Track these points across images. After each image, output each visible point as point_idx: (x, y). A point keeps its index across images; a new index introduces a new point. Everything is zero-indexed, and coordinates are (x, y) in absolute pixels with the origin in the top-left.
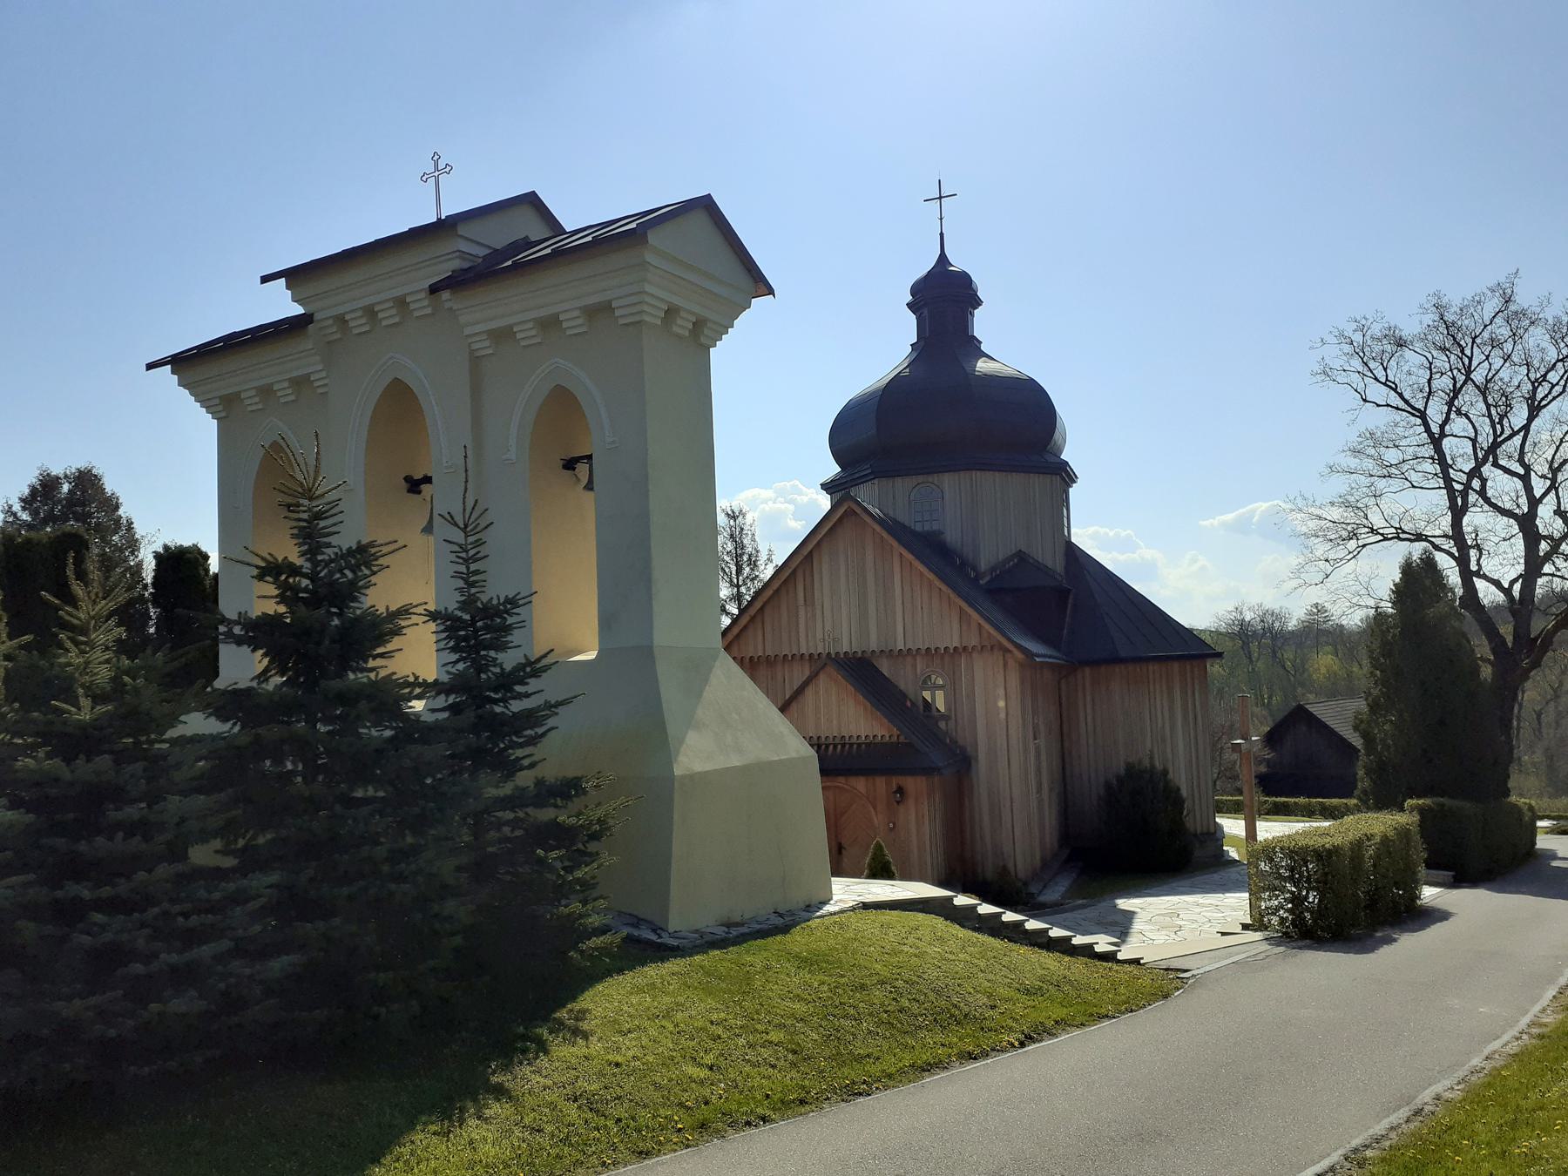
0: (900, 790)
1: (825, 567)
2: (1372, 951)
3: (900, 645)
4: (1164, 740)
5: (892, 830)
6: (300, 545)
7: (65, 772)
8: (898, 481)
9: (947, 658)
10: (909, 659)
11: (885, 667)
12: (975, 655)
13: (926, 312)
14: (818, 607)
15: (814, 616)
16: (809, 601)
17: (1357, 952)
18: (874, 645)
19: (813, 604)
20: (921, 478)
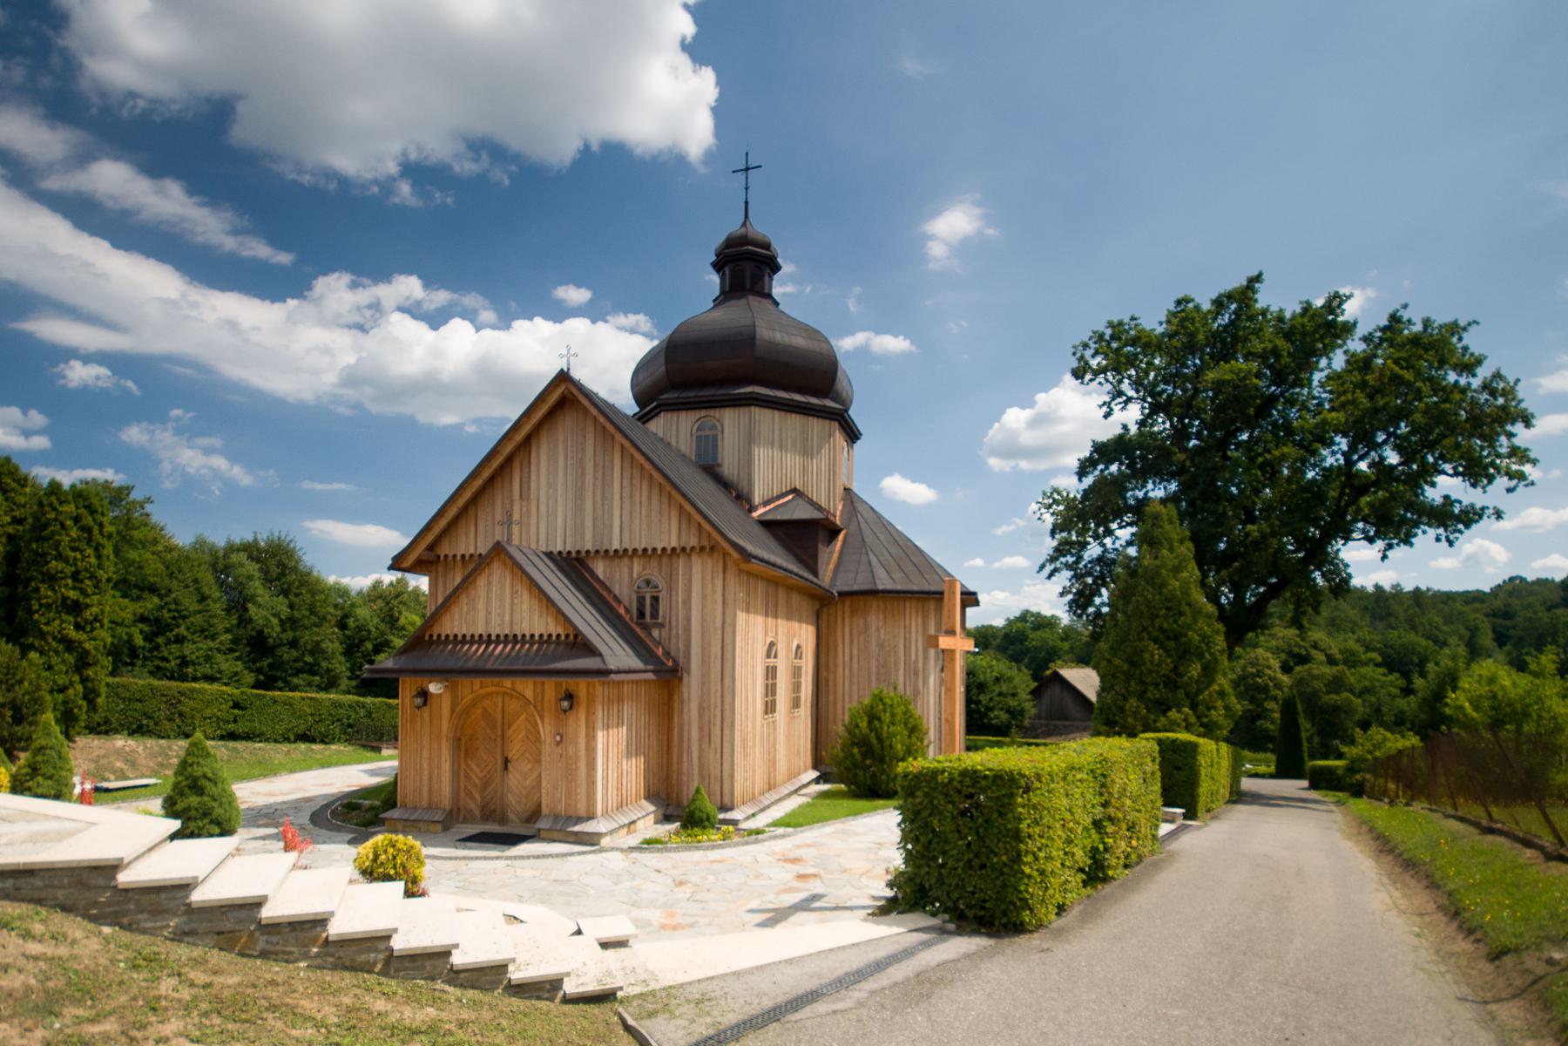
0: (570, 697)
1: (544, 457)
2: (1478, 591)
3: (616, 545)
4: (916, 673)
5: (558, 743)
6: (541, 636)
7: (418, 844)
8: (683, 415)
9: (664, 560)
10: (626, 560)
11: (600, 568)
12: (694, 558)
13: (727, 270)
14: (534, 502)
15: (529, 511)
16: (525, 496)
17: (1467, 592)
18: (589, 546)
19: (529, 498)
20: (703, 413)
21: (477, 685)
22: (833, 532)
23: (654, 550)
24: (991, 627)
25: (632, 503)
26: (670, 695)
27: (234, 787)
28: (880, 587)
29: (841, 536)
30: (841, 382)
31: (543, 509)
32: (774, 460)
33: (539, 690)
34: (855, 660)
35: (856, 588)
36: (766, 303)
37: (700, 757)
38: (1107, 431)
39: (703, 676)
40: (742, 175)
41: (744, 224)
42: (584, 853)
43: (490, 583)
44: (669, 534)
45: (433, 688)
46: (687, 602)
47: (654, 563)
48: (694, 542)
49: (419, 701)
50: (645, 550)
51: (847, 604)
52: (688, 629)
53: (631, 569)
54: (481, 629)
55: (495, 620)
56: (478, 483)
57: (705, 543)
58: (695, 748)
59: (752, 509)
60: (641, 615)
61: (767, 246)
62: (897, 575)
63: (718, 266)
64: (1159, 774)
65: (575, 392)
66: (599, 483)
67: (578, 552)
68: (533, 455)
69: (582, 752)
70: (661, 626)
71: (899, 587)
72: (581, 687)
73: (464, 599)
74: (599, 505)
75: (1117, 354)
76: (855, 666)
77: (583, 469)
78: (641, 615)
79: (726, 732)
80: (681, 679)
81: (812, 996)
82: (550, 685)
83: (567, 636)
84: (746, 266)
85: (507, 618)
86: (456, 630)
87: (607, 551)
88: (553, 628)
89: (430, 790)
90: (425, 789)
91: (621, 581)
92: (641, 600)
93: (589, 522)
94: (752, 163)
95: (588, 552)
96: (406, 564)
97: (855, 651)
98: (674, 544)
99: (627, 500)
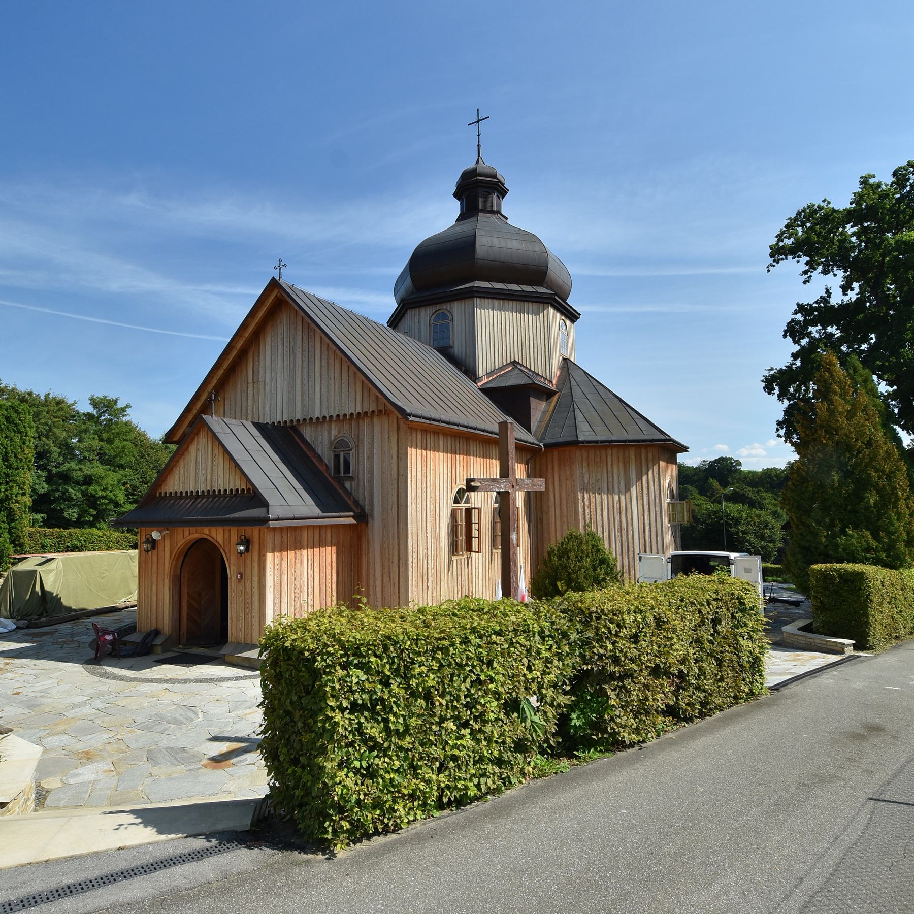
1: (268, 347)
3: (317, 414)
10: (326, 426)
14: (262, 383)
18: (299, 416)
20: (438, 307)
21: (187, 533)
22: (547, 394)
23: (345, 415)
24: (775, 469)
25: (328, 379)
26: (359, 538)
28: (581, 438)
29: (555, 398)
30: (553, 271)
31: (268, 388)
32: (500, 334)
33: (227, 536)
34: (564, 501)
35: (561, 440)
36: (493, 218)
37: (382, 591)
38: (811, 295)
39: (383, 520)
40: (475, 126)
41: (477, 162)
42: (240, 678)
43: (198, 449)
44: (354, 406)
45: (155, 535)
46: (371, 458)
47: (346, 427)
48: (373, 407)
49: (148, 546)
50: (338, 416)
51: (556, 453)
52: (371, 481)
53: (330, 433)
54: (191, 487)
55: (201, 479)
56: (221, 372)
57: (381, 407)
58: (379, 583)
59: (480, 379)
60: (337, 470)
61: (495, 176)
62: (599, 428)
63: (457, 195)
65: (285, 295)
66: (305, 365)
67: (292, 421)
68: (261, 347)
69: (256, 590)
70: (351, 479)
71: (599, 438)
72: (254, 532)
73: (182, 463)
74: (305, 382)
75: (812, 237)
76: (564, 507)
77: (295, 354)
78: (337, 470)
79: (402, 569)
80: (367, 523)
81: (70, 890)
82: (234, 531)
83: (249, 490)
84: (478, 191)
85: (209, 476)
86: (176, 489)
87: (311, 419)
88: (239, 485)
89: (157, 618)
90: (154, 617)
91: (321, 441)
92: (337, 457)
93: (299, 398)
94: (482, 116)
95: (298, 420)
96: (175, 439)
97: (564, 495)
98: (359, 410)
99: (325, 377)
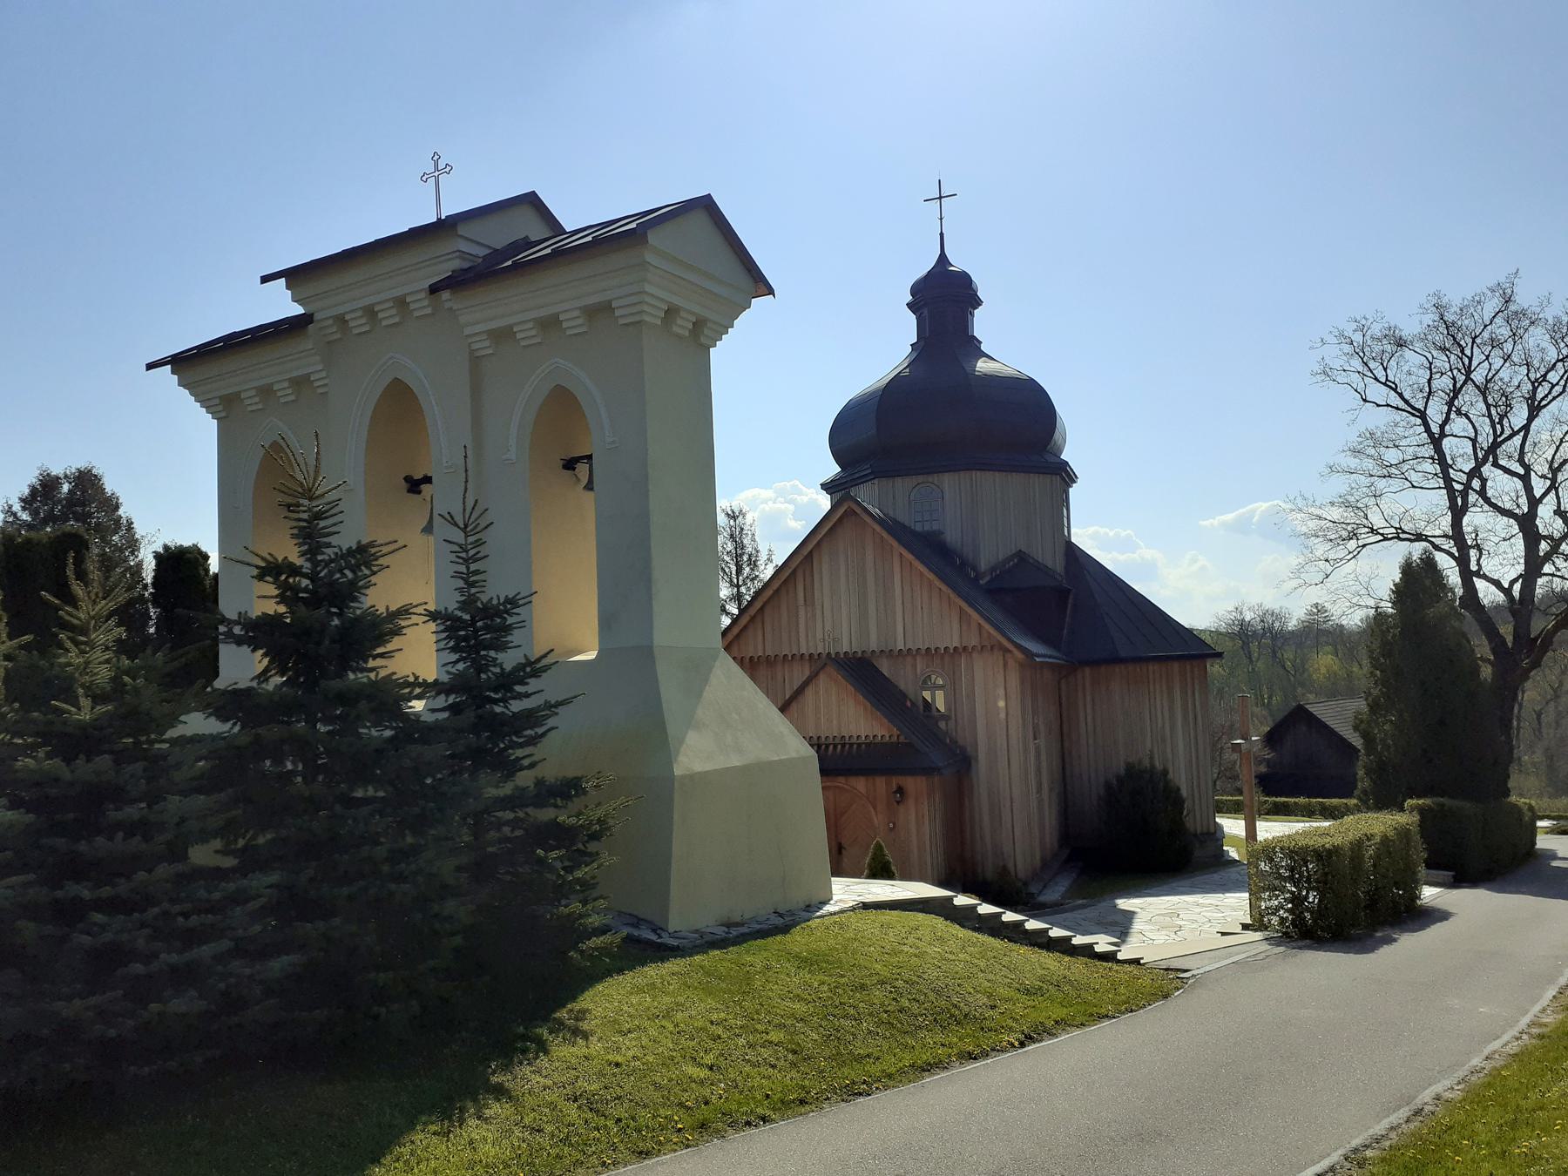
0: (900, 790)
1: (825, 567)
3: (900, 645)
4: (1164, 740)
5: (892, 830)
8: (898, 481)
9: (947, 658)
10: (909, 659)
11: (885, 667)
12: (975, 655)
13: (926, 312)
14: (818, 607)
15: (814, 616)
16: (809, 601)
17: (1357, 952)
18: (874, 645)
19: (813, 604)
20: (921, 478)
27: (1244, 834)
64: (735, 761)
